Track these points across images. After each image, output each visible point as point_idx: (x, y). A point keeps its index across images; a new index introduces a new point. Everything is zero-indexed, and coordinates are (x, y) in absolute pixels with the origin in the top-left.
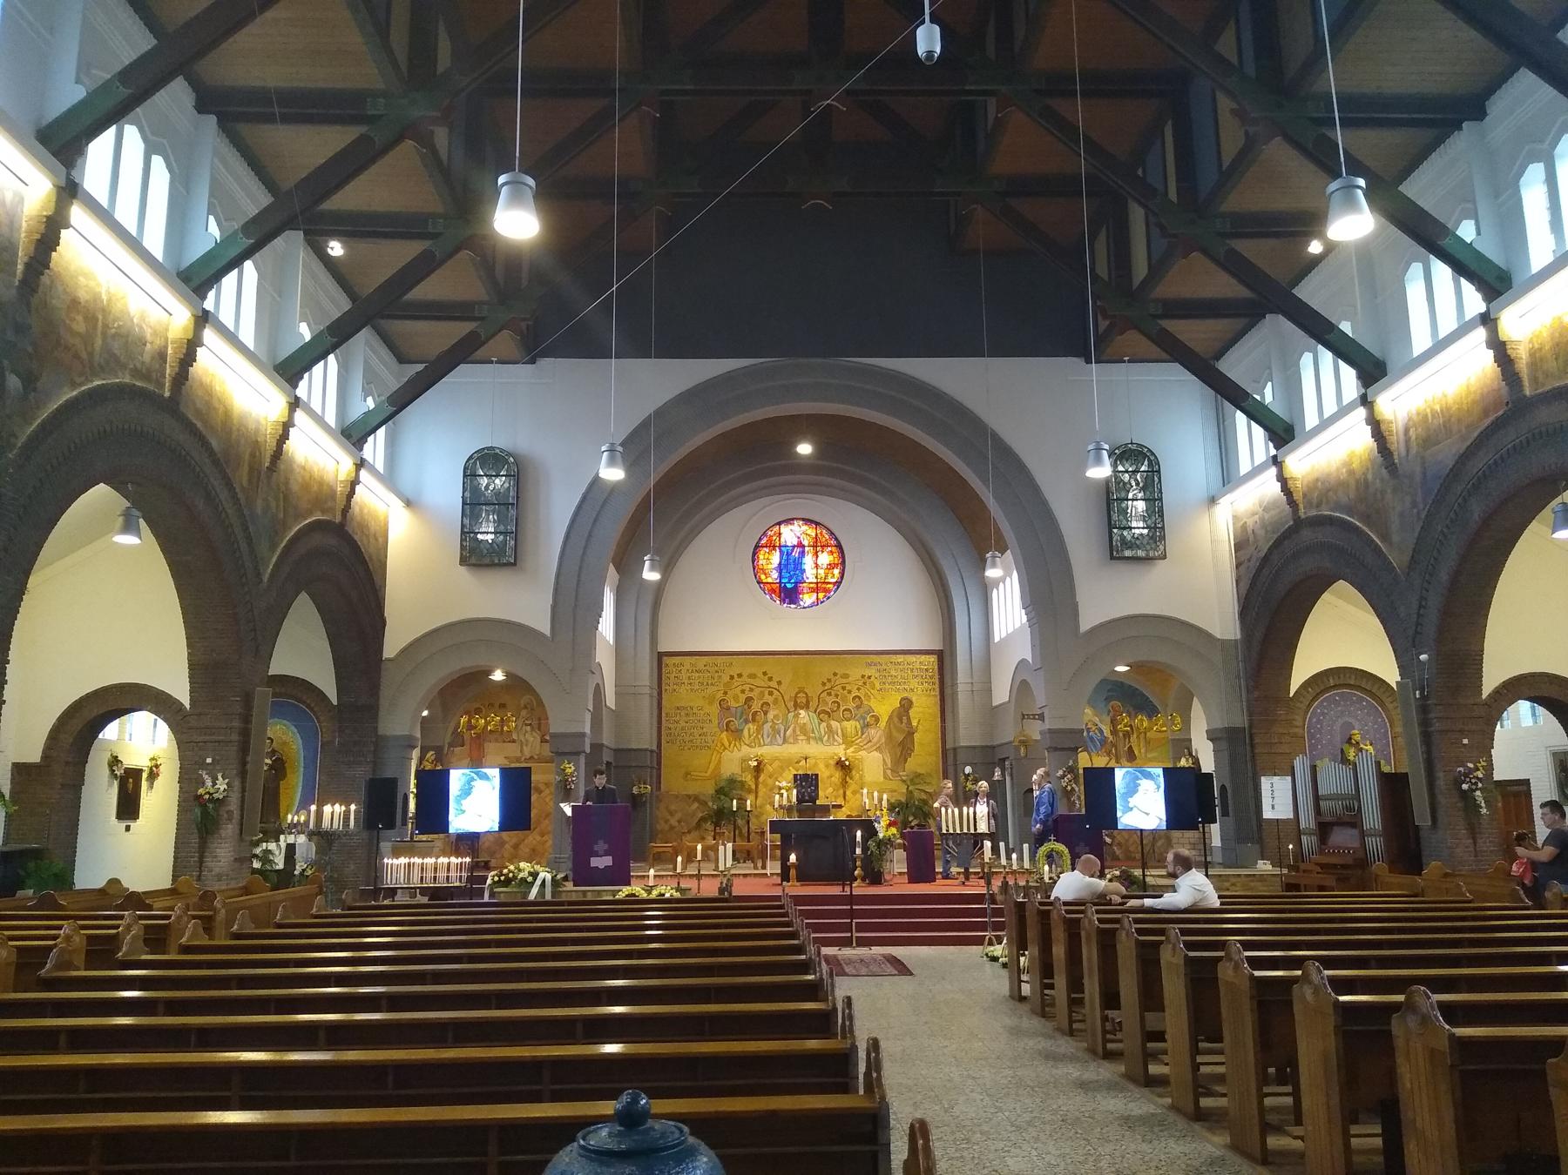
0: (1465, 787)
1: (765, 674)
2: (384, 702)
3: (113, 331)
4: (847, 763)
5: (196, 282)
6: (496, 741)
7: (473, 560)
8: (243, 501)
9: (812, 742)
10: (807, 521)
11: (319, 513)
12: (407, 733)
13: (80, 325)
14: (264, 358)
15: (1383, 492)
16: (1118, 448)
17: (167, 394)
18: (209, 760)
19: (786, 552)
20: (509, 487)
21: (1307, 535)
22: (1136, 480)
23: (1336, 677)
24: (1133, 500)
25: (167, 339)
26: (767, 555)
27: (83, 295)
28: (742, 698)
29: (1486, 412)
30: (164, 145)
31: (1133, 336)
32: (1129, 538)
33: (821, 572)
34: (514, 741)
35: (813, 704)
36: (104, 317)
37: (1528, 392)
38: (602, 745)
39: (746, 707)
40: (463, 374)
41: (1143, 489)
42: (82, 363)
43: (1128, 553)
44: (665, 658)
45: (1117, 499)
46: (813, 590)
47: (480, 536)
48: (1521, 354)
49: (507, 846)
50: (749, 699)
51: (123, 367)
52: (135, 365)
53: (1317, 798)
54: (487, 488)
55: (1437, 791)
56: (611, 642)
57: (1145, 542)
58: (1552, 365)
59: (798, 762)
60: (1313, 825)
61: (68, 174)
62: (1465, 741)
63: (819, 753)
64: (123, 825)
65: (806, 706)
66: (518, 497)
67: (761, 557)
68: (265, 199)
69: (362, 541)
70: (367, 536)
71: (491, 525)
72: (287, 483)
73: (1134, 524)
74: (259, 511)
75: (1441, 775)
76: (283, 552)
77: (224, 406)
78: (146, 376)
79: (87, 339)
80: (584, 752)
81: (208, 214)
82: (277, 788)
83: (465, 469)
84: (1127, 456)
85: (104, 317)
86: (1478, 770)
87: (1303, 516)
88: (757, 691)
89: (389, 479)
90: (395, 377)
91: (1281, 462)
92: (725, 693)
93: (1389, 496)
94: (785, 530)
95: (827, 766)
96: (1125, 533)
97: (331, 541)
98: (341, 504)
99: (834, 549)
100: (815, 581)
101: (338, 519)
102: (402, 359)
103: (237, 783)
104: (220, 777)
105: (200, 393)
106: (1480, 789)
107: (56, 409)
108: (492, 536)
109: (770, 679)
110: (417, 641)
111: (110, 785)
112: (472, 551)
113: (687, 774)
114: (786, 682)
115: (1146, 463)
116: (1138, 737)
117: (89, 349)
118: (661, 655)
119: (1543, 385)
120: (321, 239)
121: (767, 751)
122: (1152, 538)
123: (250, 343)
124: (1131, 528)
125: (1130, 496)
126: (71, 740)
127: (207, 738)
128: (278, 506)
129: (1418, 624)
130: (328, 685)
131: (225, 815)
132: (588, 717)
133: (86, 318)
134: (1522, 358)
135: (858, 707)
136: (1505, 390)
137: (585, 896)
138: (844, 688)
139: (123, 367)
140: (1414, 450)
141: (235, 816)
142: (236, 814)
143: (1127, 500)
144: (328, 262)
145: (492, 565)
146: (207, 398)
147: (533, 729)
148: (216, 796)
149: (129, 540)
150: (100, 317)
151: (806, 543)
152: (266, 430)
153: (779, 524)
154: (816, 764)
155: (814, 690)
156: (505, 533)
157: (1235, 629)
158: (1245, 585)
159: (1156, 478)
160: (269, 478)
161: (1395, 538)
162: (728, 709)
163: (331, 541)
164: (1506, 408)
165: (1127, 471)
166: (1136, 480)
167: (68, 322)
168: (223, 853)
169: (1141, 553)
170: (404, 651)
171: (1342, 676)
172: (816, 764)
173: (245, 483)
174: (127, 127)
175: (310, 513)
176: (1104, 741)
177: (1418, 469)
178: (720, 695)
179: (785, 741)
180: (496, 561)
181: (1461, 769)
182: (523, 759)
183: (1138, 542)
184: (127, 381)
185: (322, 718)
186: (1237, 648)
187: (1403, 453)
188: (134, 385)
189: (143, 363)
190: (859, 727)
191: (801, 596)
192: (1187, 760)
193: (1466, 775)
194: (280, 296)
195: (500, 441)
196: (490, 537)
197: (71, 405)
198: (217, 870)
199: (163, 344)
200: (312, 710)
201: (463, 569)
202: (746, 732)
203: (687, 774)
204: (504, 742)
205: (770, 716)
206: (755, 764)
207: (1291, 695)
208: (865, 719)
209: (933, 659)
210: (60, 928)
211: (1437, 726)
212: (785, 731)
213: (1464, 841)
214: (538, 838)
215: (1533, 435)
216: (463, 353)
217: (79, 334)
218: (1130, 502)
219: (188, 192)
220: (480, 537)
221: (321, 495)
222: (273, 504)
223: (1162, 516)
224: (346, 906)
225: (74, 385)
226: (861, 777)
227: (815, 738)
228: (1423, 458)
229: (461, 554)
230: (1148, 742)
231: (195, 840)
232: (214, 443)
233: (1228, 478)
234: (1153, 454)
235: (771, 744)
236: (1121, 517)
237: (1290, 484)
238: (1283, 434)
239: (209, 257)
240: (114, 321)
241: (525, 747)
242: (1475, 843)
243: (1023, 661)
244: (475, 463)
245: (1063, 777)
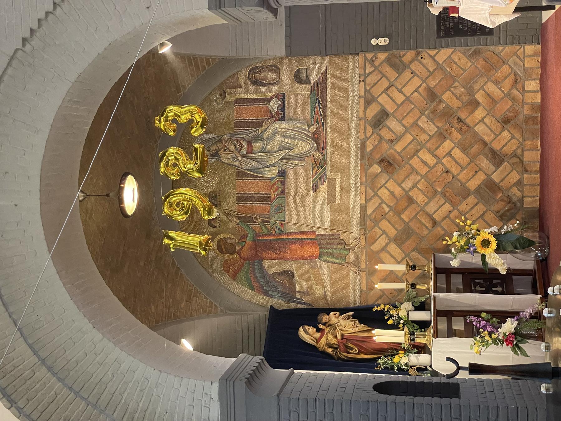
12: (216, 386)
34: (282, 174)
49: (496, 177)
147: (259, 138)
182: (317, 155)
204: (283, 192)
214: (479, 113)
224: (45, 19)
225: (334, 375)
241: (296, 152)
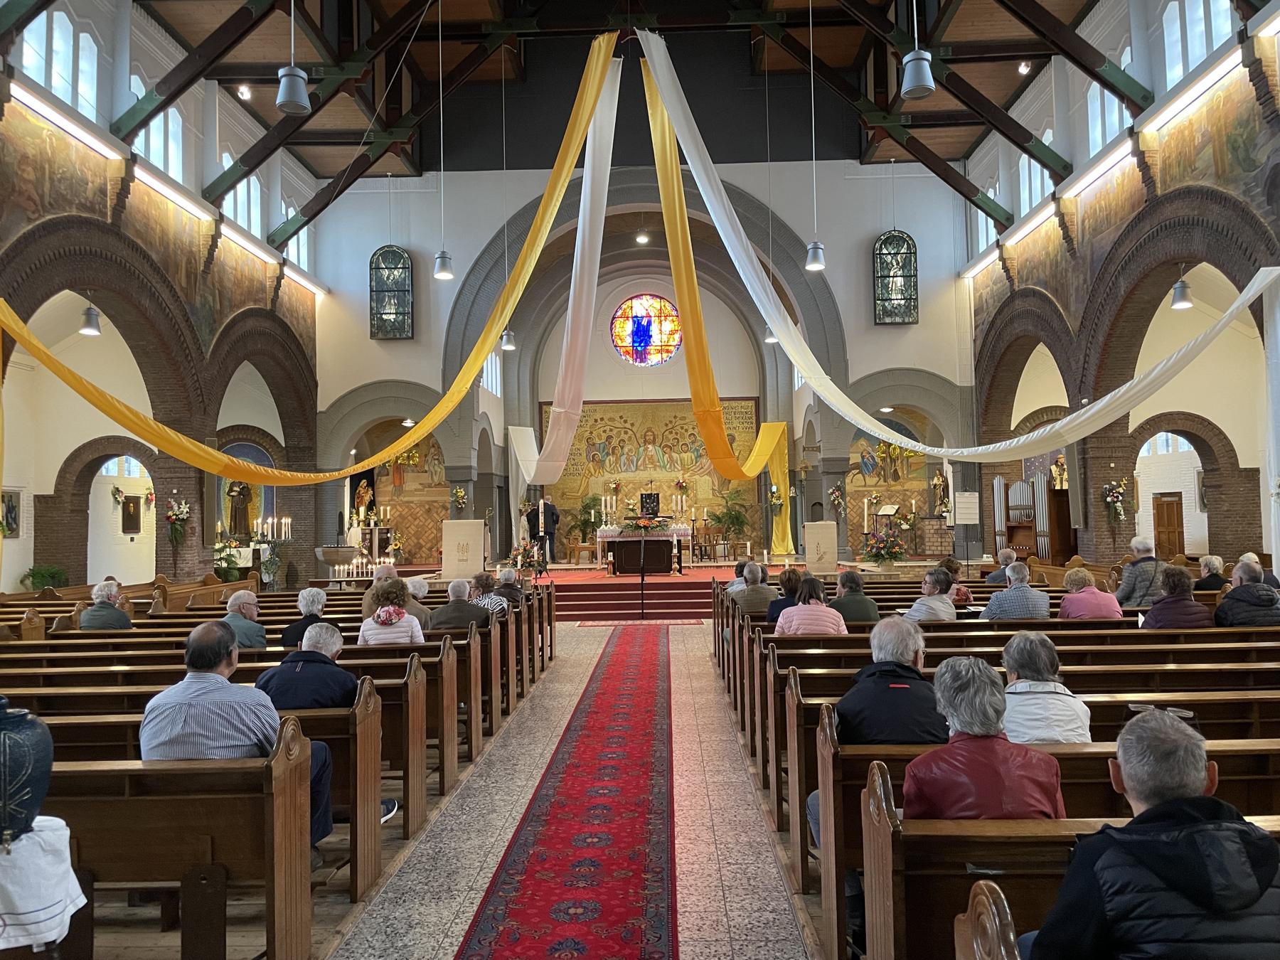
0: (1109, 499)
1: (621, 417)
2: (320, 446)
3: (59, 176)
4: (684, 484)
5: (124, 133)
6: (413, 471)
7: (380, 335)
8: (183, 298)
9: (658, 469)
10: (653, 296)
11: (252, 303)
13: (30, 174)
14: (192, 188)
15: (1067, 270)
16: (883, 235)
17: (109, 221)
18: (175, 491)
19: (637, 321)
20: (405, 278)
21: (1019, 304)
22: (897, 261)
23: (1049, 414)
24: (893, 277)
25: (105, 179)
26: (622, 325)
27: (31, 151)
28: (604, 436)
29: (1133, 208)
30: (90, 24)
31: (888, 143)
32: (889, 308)
33: (665, 338)
34: (426, 472)
35: (659, 441)
36: (50, 166)
37: (1159, 192)
38: (492, 474)
39: (607, 443)
40: (361, 186)
41: (903, 268)
42: (35, 204)
43: (888, 320)
44: (544, 407)
45: (881, 276)
46: (660, 351)
47: (384, 316)
48: (1156, 162)
50: (609, 437)
51: (70, 203)
52: (80, 201)
53: (1008, 508)
54: (388, 278)
55: (1089, 503)
56: (499, 396)
57: (902, 311)
58: (1175, 171)
59: (647, 485)
60: (1004, 529)
61: (5, 61)
62: (1112, 465)
63: (660, 478)
64: (129, 536)
65: (654, 442)
66: (412, 285)
67: (618, 326)
68: (180, 55)
69: (291, 322)
70: (297, 319)
71: (393, 307)
72: (221, 281)
73: (894, 297)
74: (198, 304)
75: (1092, 491)
76: (221, 335)
77: (161, 226)
78: (91, 209)
79: (38, 183)
80: (471, 480)
81: (131, 74)
82: (246, 509)
83: (371, 263)
84: (890, 241)
85: (50, 166)
86: (1121, 486)
87: (1017, 289)
88: (615, 431)
89: (314, 275)
90: (309, 188)
91: (1002, 246)
92: (591, 433)
93: (1069, 274)
94: (636, 302)
95: (669, 487)
96: (887, 304)
97: (266, 325)
98: (270, 295)
99: (675, 318)
100: (660, 344)
101: (269, 307)
102: (318, 176)
103: (197, 507)
104: (183, 503)
105: (139, 217)
106: (1121, 501)
107: (17, 240)
108: (394, 316)
109: (625, 422)
110: (343, 397)
111: (115, 508)
112: (379, 328)
113: (563, 494)
114: (637, 424)
115: (905, 246)
116: (901, 462)
117: (40, 192)
118: (541, 404)
119: (1169, 187)
120: (233, 86)
121: (622, 476)
122: (907, 307)
123: (179, 179)
124: (891, 300)
125: (892, 274)
126: (74, 478)
127: (173, 475)
128: (214, 300)
129: (1084, 375)
130: (276, 430)
131: (190, 531)
132: (474, 454)
133: (35, 169)
134: (1156, 165)
135: (693, 443)
136: (1145, 190)
137: (434, 587)
138: (682, 428)
139: (70, 203)
140: (1086, 238)
141: (197, 530)
142: (198, 529)
143: (889, 277)
144: (243, 104)
145: (394, 339)
146: (145, 220)
148: (181, 516)
149: (90, 332)
150: (47, 166)
151: (652, 314)
152: (199, 242)
153: (631, 299)
154: (660, 486)
155: (659, 430)
156: (403, 314)
157: (971, 378)
158: (979, 342)
159: (913, 259)
160: (205, 279)
161: (1073, 309)
162: (594, 444)
163: (266, 325)
164: (1145, 205)
165: (890, 254)
166: (897, 261)
167: (19, 173)
168: (191, 557)
169: (898, 320)
170: (332, 406)
171: (1054, 413)
172: (660, 486)
173: (184, 284)
174: (56, 14)
175: (243, 303)
176: (875, 465)
177: (1089, 253)
178: (587, 434)
179: (637, 469)
180: (398, 336)
181: (1107, 486)
183: (896, 311)
184: (74, 213)
185: (275, 457)
186: (972, 391)
187: (1080, 240)
188: (80, 216)
189: (86, 199)
190: (693, 457)
191: (649, 357)
192: (939, 479)
193: (1111, 490)
194: (203, 135)
195: (397, 241)
196: (392, 317)
197: (27, 238)
198: (187, 569)
199: (102, 182)
200: (267, 450)
201: (373, 342)
202: (607, 461)
203: (563, 494)
205: (626, 450)
206: (614, 486)
207: (1012, 429)
208: (698, 451)
209: (751, 403)
210: (23, 613)
211: (1091, 454)
212: (638, 461)
213: (1106, 540)
215: (1161, 227)
216: (360, 169)
217: (30, 181)
218: (891, 279)
219: (114, 60)
220: (385, 317)
221: (254, 290)
222: (210, 299)
223: (916, 290)
225: (30, 220)
226: (695, 496)
227: (660, 466)
228: (1092, 245)
229: (371, 331)
230: (909, 466)
231: (169, 548)
232: (154, 256)
233: (971, 256)
234: (911, 239)
235: (626, 471)
236: (884, 291)
237: (1008, 263)
238: (1005, 222)
239: (132, 111)
240: (59, 168)
242: (1114, 541)
243: (810, 405)
244: (378, 258)
245: (832, 494)
